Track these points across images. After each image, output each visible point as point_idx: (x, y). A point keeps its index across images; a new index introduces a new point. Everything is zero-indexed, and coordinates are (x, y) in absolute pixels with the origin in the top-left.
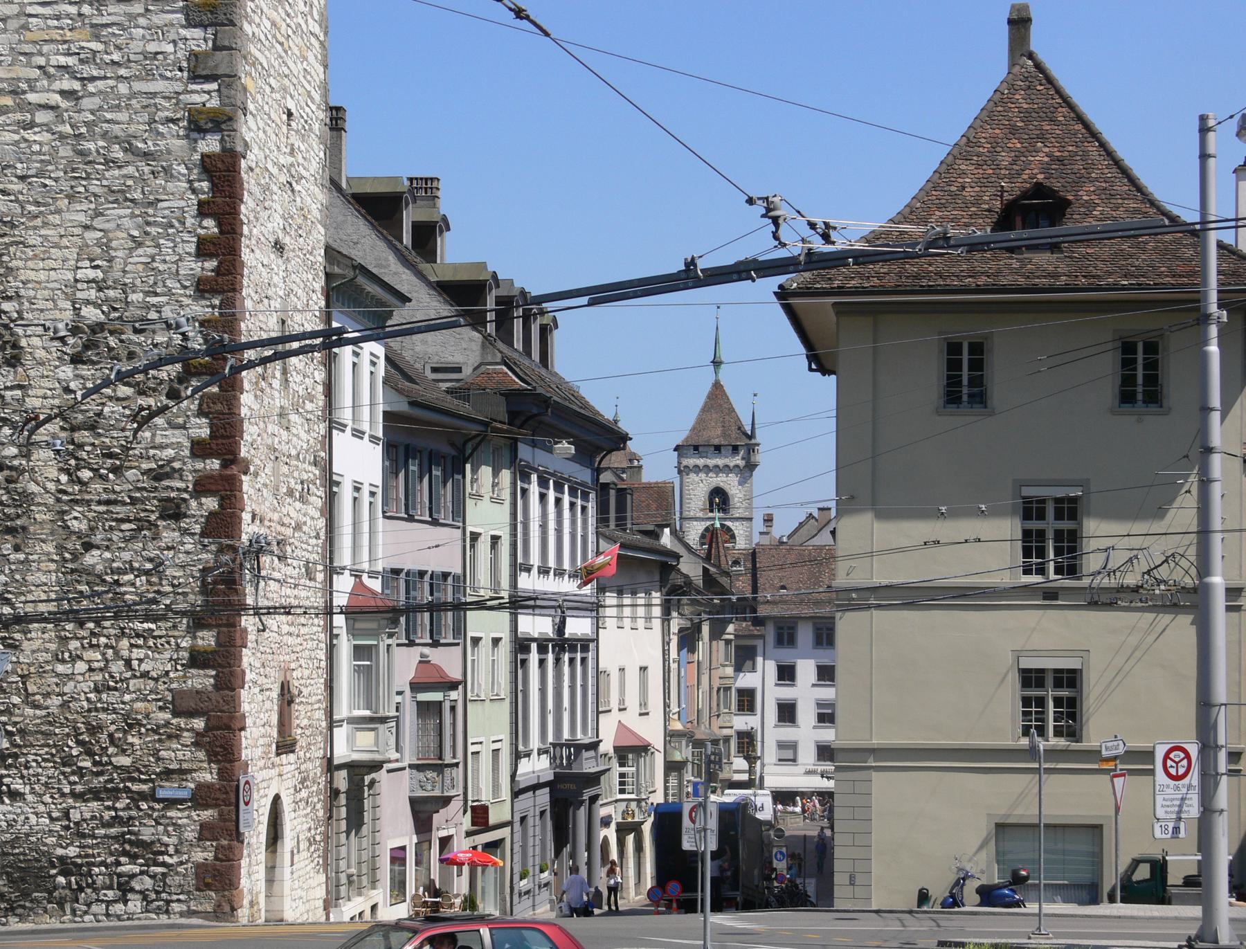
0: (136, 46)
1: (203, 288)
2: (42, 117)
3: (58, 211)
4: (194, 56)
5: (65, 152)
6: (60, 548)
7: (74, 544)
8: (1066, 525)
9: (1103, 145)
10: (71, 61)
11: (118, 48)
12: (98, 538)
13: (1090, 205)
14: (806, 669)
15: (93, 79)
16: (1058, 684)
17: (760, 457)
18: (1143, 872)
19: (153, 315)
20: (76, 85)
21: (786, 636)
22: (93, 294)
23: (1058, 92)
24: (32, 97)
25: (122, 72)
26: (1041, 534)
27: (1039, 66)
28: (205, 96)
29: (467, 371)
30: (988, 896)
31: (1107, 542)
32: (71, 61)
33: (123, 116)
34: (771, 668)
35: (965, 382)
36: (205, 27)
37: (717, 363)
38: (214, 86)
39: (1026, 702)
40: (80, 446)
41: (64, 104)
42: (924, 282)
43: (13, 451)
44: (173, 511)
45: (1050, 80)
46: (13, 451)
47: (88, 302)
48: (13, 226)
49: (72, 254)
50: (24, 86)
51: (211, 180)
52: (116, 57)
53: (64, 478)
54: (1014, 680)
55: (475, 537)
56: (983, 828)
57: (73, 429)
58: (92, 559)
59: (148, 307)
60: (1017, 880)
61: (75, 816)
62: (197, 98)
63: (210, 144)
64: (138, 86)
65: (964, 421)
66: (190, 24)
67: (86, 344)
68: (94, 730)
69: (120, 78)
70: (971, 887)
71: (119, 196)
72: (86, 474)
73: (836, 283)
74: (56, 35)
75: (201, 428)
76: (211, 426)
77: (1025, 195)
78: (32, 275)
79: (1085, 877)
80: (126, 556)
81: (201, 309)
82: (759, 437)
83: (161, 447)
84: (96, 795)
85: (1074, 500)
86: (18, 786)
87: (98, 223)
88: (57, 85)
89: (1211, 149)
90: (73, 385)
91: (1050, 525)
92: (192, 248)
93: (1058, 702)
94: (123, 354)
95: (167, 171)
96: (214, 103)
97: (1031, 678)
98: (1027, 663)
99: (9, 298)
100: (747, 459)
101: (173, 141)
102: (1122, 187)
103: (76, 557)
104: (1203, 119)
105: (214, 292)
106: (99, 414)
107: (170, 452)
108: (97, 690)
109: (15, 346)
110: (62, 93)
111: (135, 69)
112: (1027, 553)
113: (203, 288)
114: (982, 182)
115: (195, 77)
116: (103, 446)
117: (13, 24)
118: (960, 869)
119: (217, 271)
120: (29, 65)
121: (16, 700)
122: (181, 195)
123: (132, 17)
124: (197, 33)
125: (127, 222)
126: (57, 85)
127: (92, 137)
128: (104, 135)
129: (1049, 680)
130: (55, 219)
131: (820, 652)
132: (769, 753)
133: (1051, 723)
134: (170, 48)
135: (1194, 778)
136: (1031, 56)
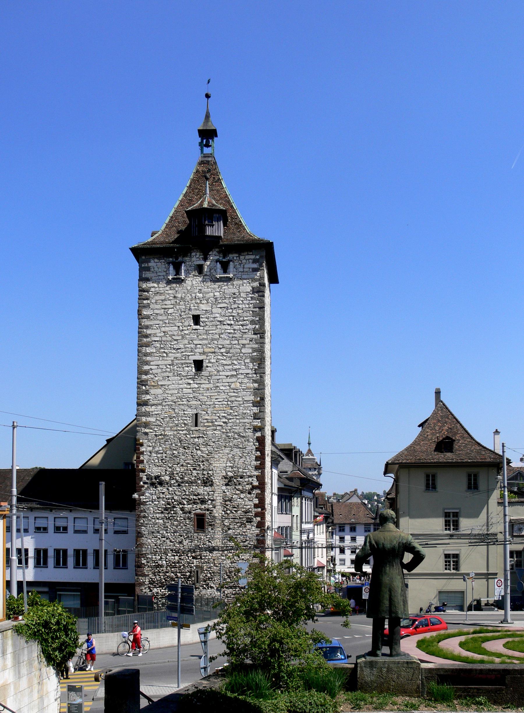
0: (241, 411)
1: (257, 468)
2: (218, 428)
3: (222, 450)
4: (255, 414)
5: (224, 436)
6: (223, 529)
7: (226, 528)
8: (455, 519)
9: (461, 425)
10: (225, 415)
11: (237, 412)
12: (231, 526)
13: (459, 440)
14: (348, 538)
15: (230, 419)
16: (453, 557)
17: (322, 471)
18: (475, 603)
19: (245, 474)
20: (227, 420)
21: (342, 529)
22: (230, 469)
23: (449, 411)
24: (216, 423)
25: (237, 417)
26: (449, 521)
27: (444, 404)
28: (257, 423)
29: (289, 472)
30: (437, 609)
31: (466, 524)
32: (225, 415)
33: (238, 428)
34: (338, 538)
35: (431, 485)
36: (257, 407)
37: (309, 444)
38: (260, 421)
39: (446, 562)
40: (227, 505)
41: (224, 425)
42: (421, 461)
43: (211, 506)
44: (250, 521)
45: (447, 408)
46: (211, 506)
47: (229, 471)
48: (211, 453)
49: (225, 460)
50: (214, 421)
51: (259, 443)
52: (236, 414)
53: (223, 513)
54: (443, 556)
55: (293, 516)
56: (435, 593)
57: (226, 501)
58: (230, 532)
59: (243, 472)
60: (444, 605)
61: (226, 592)
62: (255, 423)
63: (259, 434)
64: (241, 421)
65: (431, 495)
66: (254, 406)
67: (229, 481)
68: (230, 572)
69: (237, 419)
70: (433, 606)
71: (237, 447)
72: (229, 512)
73: (400, 461)
74: (222, 409)
75: (256, 501)
76: (259, 500)
77: (444, 439)
78: (216, 465)
79: (459, 603)
80: (238, 531)
81: (256, 473)
82: (322, 466)
83: (247, 505)
84: (231, 587)
85: (457, 513)
86: (212, 585)
87: (232, 452)
88: (222, 420)
89: (505, 450)
90: (225, 491)
91: (451, 519)
92: (254, 458)
93: (453, 562)
94: (238, 483)
95: (248, 440)
96: (260, 425)
97: (447, 556)
98: (446, 552)
99: (210, 470)
100: (318, 472)
101: (250, 433)
102: (466, 435)
103: (226, 531)
104: (503, 444)
105: (259, 469)
106: (232, 498)
107: (249, 507)
108: (231, 563)
109: (212, 481)
110: (223, 422)
111: (241, 417)
112: (446, 526)
113: (257, 468)
114: (433, 434)
115: (255, 419)
116: (233, 505)
117: (212, 406)
118: (430, 603)
119: (260, 464)
120: (215, 416)
121: (212, 565)
122: (252, 446)
123: (240, 405)
124: (255, 408)
125: (238, 452)
126: (222, 420)
127: (230, 433)
128: (233, 432)
129: (451, 556)
130: (221, 452)
131: (351, 533)
132: (337, 562)
133: (452, 567)
134: (249, 412)
135: (503, 586)
136: (442, 402)
